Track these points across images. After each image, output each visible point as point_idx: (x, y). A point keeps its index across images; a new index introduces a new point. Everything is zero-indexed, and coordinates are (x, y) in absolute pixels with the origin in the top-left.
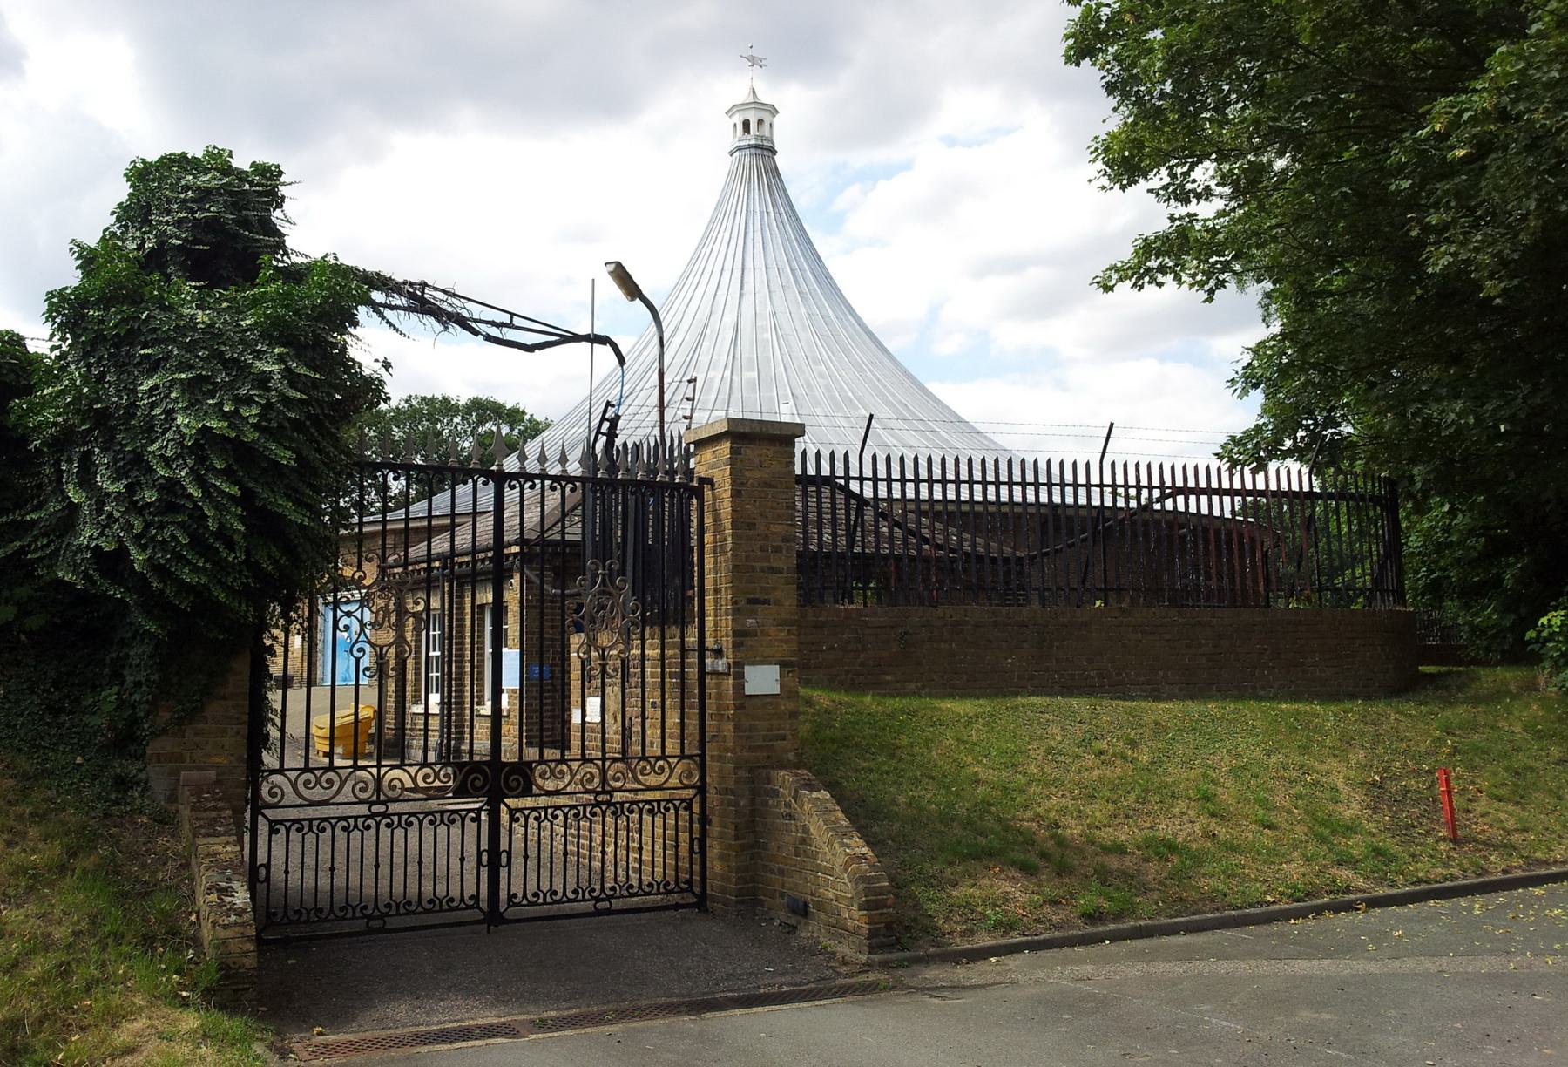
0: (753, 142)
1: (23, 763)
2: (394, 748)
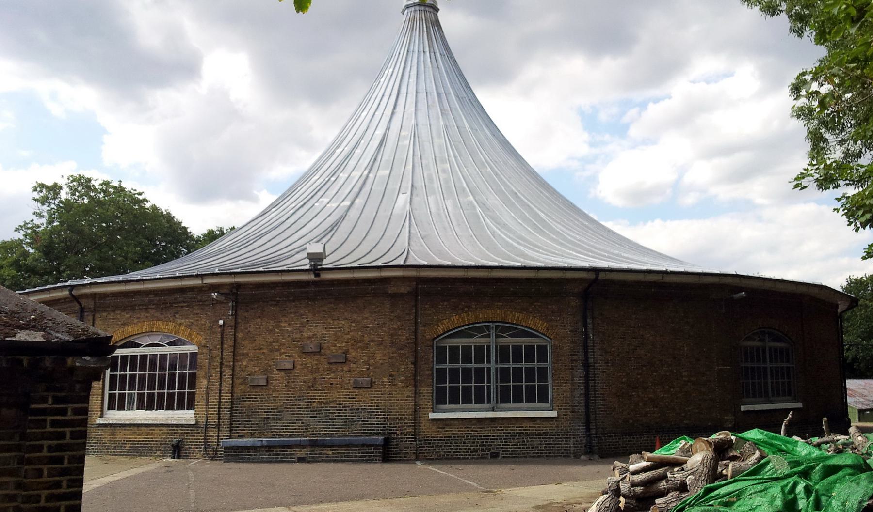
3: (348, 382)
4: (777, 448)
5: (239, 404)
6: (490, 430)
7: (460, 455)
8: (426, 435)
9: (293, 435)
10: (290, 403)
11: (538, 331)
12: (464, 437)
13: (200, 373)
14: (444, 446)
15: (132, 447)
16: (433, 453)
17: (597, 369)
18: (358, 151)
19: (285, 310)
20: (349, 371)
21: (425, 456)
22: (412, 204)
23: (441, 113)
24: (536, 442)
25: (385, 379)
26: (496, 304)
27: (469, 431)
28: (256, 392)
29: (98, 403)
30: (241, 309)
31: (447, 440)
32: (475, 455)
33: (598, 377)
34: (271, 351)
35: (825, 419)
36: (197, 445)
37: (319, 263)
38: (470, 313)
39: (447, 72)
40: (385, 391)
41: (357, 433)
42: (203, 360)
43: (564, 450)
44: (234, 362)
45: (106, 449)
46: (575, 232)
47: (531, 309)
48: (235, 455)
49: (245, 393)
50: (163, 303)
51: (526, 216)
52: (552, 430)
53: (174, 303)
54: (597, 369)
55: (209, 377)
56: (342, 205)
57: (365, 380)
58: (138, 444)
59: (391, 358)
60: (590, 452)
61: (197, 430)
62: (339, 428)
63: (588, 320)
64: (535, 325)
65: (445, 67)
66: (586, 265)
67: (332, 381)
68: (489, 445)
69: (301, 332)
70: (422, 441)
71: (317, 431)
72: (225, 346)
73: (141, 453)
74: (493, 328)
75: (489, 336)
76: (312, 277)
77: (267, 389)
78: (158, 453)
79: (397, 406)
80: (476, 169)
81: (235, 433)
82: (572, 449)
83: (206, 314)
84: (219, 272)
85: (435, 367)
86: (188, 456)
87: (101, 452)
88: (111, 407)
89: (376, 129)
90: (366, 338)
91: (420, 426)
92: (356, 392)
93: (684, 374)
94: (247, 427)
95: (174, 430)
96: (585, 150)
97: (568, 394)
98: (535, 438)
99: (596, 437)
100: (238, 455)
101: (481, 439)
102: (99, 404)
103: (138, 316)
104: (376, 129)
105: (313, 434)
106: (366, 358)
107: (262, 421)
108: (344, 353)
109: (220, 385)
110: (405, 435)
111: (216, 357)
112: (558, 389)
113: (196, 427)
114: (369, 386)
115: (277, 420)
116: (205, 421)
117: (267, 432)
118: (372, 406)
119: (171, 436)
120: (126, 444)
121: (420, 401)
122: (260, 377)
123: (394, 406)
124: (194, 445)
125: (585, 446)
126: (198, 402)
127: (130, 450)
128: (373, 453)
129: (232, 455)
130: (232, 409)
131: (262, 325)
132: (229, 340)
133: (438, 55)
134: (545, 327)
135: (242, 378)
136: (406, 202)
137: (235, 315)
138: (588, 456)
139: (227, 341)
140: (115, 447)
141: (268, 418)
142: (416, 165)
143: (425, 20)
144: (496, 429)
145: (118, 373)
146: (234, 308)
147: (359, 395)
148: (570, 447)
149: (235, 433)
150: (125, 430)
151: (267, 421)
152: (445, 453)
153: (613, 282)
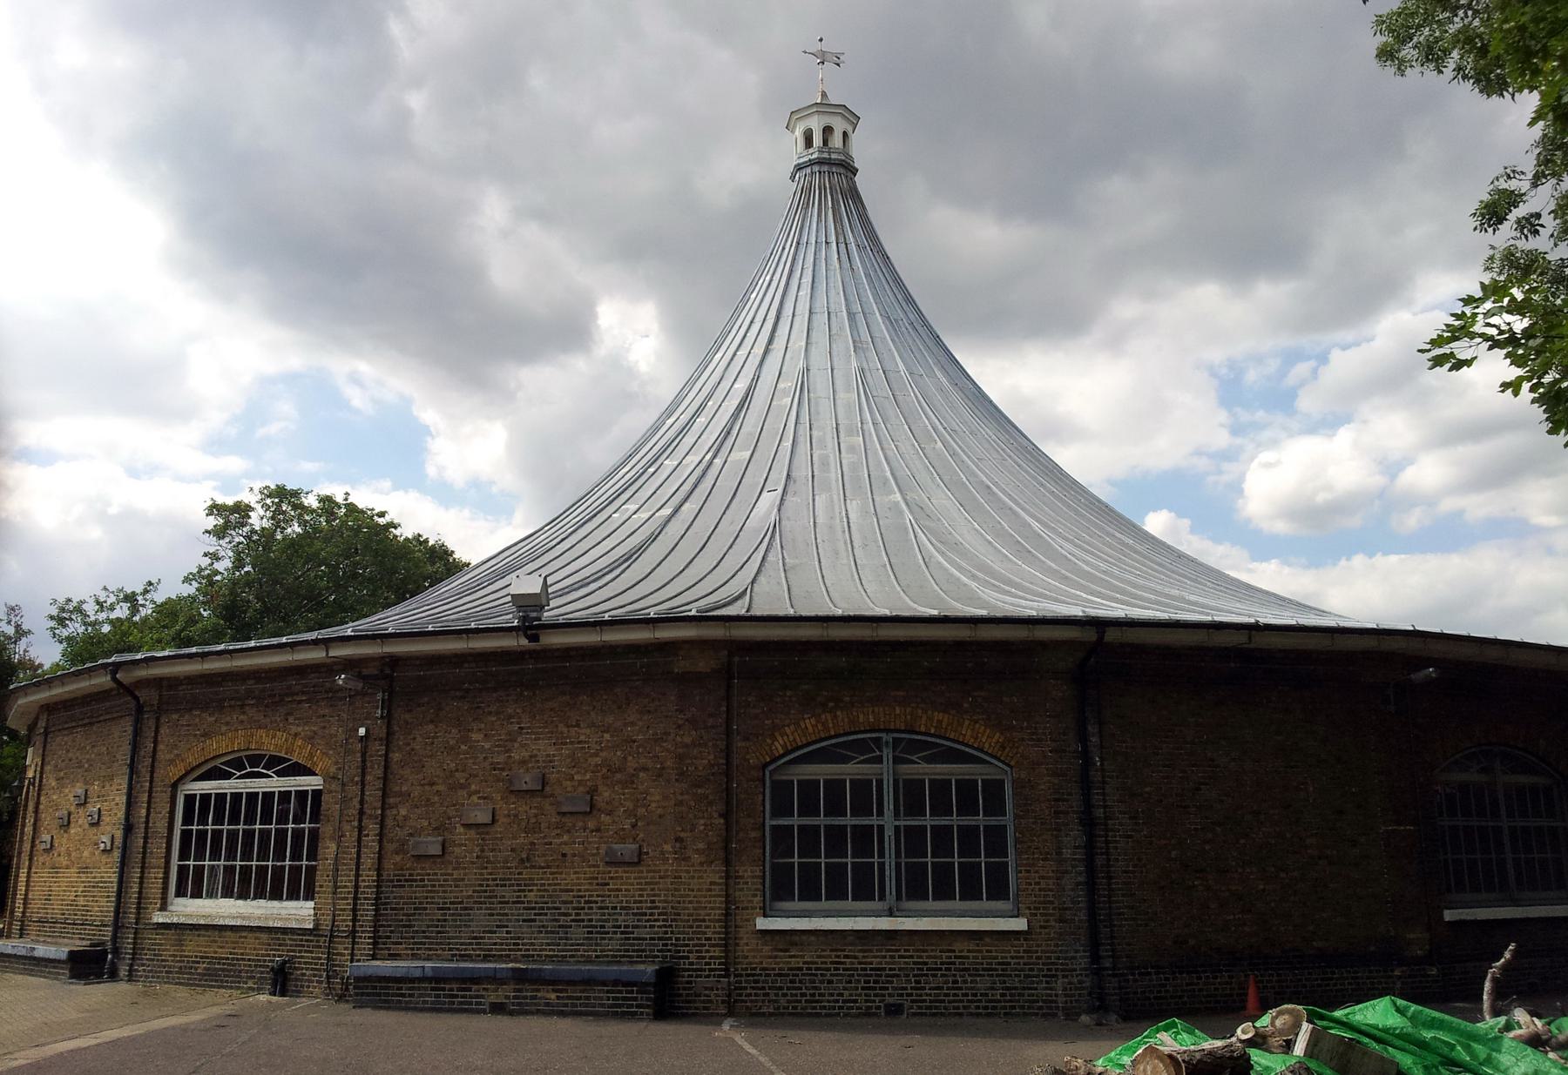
3: (595, 851)
4: (1439, 1055)
5: (392, 892)
6: (885, 957)
7: (821, 1008)
8: (751, 963)
9: (490, 956)
10: (486, 891)
11: (982, 751)
12: (829, 969)
13: (326, 829)
14: (788, 989)
15: (208, 969)
16: (763, 1001)
17: (1112, 830)
18: (702, 420)
19: (479, 707)
20: (598, 830)
21: (747, 1008)
22: (782, 511)
23: (854, 347)
24: (982, 984)
25: (668, 847)
26: (892, 694)
27: (838, 957)
28: (423, 869)
29: (157, 883)
30: (399, 706)
31: (793, 975)
32: (852, 1008)
33: (1116, 848)
34: (452, 788)
36: (316, 970)
37: (534, 615)
38: (839, 713)
39: (867, 275)
40: (667, 870)
41: (613, 956)
42: (330, 805)
43: (1044, 1001)
44: (383, 809)
45: (167, 972)
46: (1099, 557)
47: (966, 705)
48: (373, 994)
49: (402, 869)
50: (270, 696)
51: (1004, 528)
52: (1017, 957)
53: (287, 695)
54: (1112, 830)
55: (339, 838)
56: (657, 514)
57: (627, 849)
58: (219, 963)
59: (680, 803)
60: (1099, 1008)
61: (318, 941)
62: (578, 945)
63: (1090, 728)
64: (976, 739)
65: (865, 267)
66: (1076, 611)
67: (566, 850)
68: (881, 989)
69: (507, 752)
70: (741, 975)
71: (536, 950)
72: (368, 778)
73: (222, 981)
74: (887, 742)
75: (879, 760)
77: (443, 863)
78: (250, 984)
79: (690, 902)
80: (914, 445)
81: (382, 949)
82: (1061, 999)
83: (339, 716)
84: (353, 634)
85: (769, 823)
86: (299, 992)
87: (158, 977)
88: (180, 893)
89: (735, 380)
90: (632, 763)
91: (737, 945)
92: (610, 872)
93: (1308, 841)
94: (406, 938)
95: (278, 939)
96: (1222, 439)
97: (1051, 882)
98: (980, 975)
99: (1114, 975)
100: (379, 995)
101: (867, 975)
102: (160, 886)
103: (228, 719)
104: (735, 380)
105: (528, 956)
106: (630, 805)
107: (432, 926)
108: (588, 793)
109: (359, 853)
110: (706, 964)
111: (352, 798)
112: (1028, 871)
113: (315, 936)
114: (636, 860)
115: (460, 926)
116: (330, 923)
117: (444, 950)
118: (641, 902)
119: (275, 950)
120: (198, 962)
121: (737, 893)
122: (430, 838)
123: (684, 902)
124: (312, 969)
125: (1090, 994)
126: (321, 886)
127: (205, 975)
128: (635, 999)
129: (368, 995)
130: (378, 901)
131: (437, 737)
132: (376, 766)
133: (853, 247)
134: (998, 741)
135: (398, 841)
137: (388, 719)
138: (1095, 1016)
139: (372, 768)
140: (181, 968)
141: (445, 920)
142: (801, 439)
143: (831, 188)
144: (897, 954)
145: (194, 828)
146: (386, 704)
147: (617, 878)
148: (1056, 995)
149: (382, 949)
150: (199, 936)
151: (442, 926)
152: (788, 1002)
153: (1139, 649)
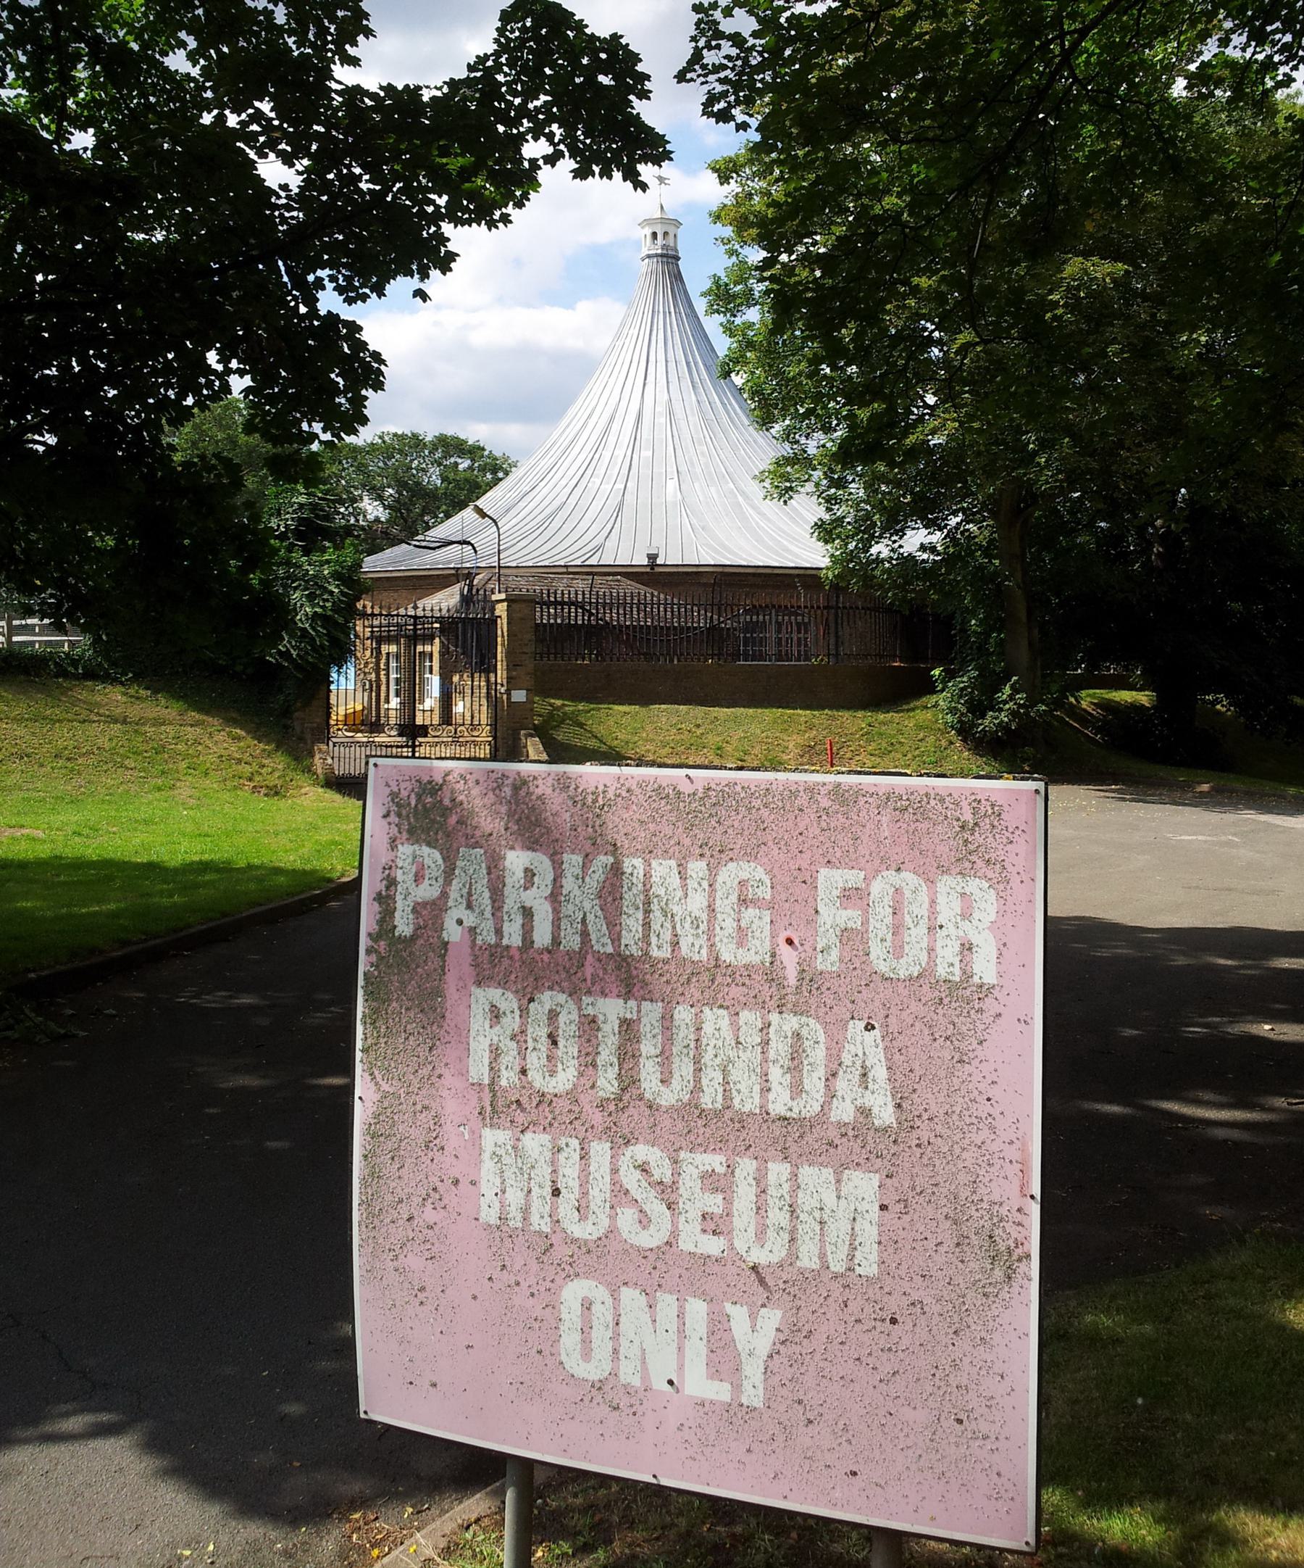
0: (659, 251)
1: (256, 720)
2: (376, 727)
18: (615, 426)
35: (77, 369)
76: (648, 570)
136: (676, 493)
